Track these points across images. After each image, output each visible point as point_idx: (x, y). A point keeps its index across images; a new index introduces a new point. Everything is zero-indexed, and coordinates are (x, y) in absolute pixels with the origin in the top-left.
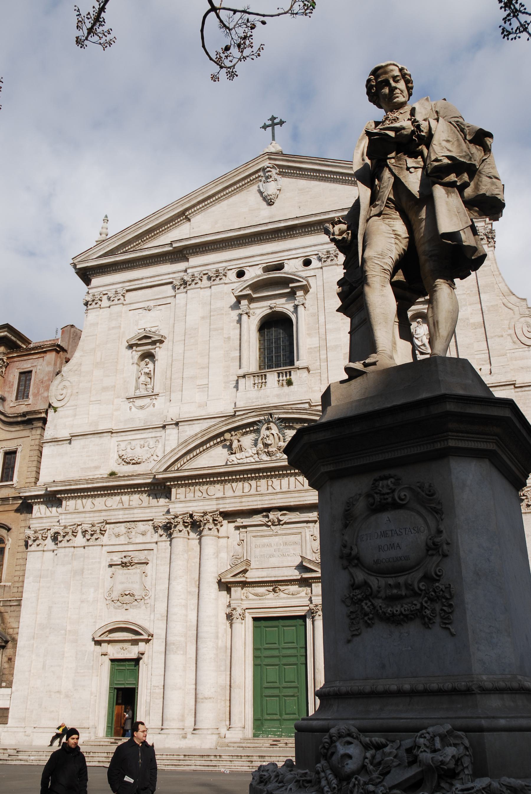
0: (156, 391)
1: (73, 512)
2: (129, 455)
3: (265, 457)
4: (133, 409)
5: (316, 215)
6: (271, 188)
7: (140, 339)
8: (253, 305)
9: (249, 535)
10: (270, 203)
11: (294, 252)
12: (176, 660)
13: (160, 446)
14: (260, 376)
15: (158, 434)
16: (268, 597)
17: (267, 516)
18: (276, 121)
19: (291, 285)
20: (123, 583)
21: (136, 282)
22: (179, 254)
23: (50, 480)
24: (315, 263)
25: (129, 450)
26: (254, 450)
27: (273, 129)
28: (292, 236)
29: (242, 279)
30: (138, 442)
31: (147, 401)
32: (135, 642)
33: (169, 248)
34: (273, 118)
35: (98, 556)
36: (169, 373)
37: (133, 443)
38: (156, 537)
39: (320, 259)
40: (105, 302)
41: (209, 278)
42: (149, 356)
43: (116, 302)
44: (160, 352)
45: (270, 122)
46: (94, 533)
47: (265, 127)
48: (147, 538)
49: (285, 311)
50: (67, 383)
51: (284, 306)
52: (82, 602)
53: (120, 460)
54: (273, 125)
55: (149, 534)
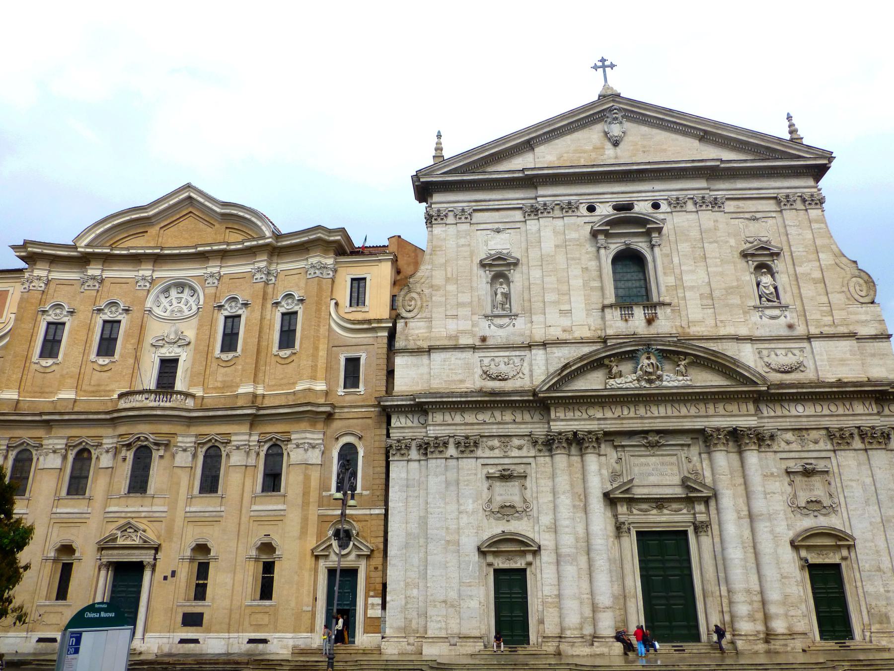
0: (514, 311)
1: (438, 426)
2: (493, 371)
3: (643, 384)
4: (492, 327)
5: (702, 161)
6: (615, 130)
7: (493, 260)
9: (627, 454)
10: (616, 144)
11: (644, 194)
12: (569, 571)
15: (523, 353)
16: (652, 512)
17: (647, 438)
18: (607, 63)
19: (648, 226)
20: (501, 495)
21: (483, 203)
23: (404, 388)
24: (664, 207)
25: (493, 366)
26: (634, 377)
27: (604, 71)
29: (593, 214)
30: (501, 359)
31: (506, 321)
32: (523, 553)
33: (521, 175)
34: (603, 60)
35: (471, 470)
37: (497, 360)
38: (533, 453)
39: (670, 204)
40: (451, 219)
41: (562, 209)
42: (762, 268)
43: (463, 220)
45: (600, 64)
46: (468, 446)
48: (524, 452)
49: (639, 248)
50: (414, 295)
51: (641, 245)
52: (460, 513)
53: (485, 376)
55: (525, 448)
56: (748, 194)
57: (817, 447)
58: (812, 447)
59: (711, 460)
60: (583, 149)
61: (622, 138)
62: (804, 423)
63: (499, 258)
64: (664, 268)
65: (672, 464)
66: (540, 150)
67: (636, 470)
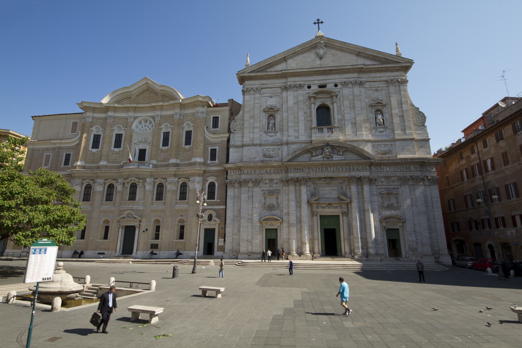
6: (321, 52)
8: (316, 100)
10: (321, 58)
13: (280, 151)
22: (284, 75)
24: (339, 86)
28: (331, 74)
34: (318, 20)
36: (281, 123)
39: (342, 84)
42: (379, 111)
44: (278, 117)
45: (317, 22)
47: (315, 23)
51: (328, 103)
54: (318, 23)
56: (375, 79)
57: (394, 184)
58: (391, 183)
60: (308, 61)
63: (379, 103)
65: (335, 190)
66: (290, 61)
67: (321, 192)
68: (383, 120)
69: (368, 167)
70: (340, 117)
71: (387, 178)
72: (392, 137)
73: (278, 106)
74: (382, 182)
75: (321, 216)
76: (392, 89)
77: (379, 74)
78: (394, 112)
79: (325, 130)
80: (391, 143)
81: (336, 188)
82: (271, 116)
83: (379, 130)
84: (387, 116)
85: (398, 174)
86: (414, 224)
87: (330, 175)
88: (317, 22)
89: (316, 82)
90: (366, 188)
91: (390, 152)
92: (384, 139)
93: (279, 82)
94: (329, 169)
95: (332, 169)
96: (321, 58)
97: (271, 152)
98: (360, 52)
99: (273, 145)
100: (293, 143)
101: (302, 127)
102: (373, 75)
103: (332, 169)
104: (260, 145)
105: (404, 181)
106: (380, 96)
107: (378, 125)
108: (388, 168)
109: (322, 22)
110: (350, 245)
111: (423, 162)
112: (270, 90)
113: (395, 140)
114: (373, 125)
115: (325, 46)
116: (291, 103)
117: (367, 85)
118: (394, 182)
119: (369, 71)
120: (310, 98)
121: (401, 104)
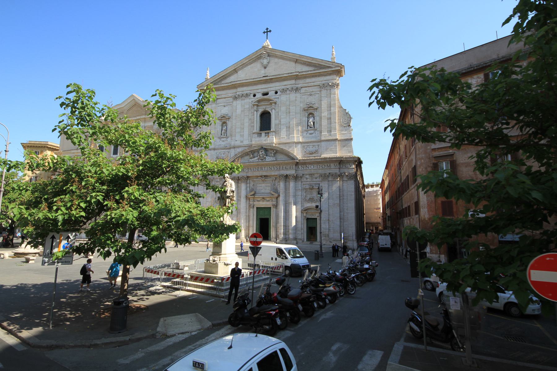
6: (265, 61)
14: (260, 135)
22: (234, 86)
34: (267, 29)
42: (311, 115)
44: (229, 123)
47: (264, 33)
54: (267, 32)
56: (310, 84)
58: (314, 180)
59: (368, 186)
60: (254, 71)
61: (267, 65)
62: (313, 172)
63: (224, 117)
64: (275, 117)
66: (240, 72)
67: (258, 188)
68: (314, 123)
69: (294, 166)
70: (277, 122)
71: (311, 175)
72: (319, 138)
73: (230, 115)
74: (307, 179)
75: (257, 208)
76: (324, 92)
77: (313, 79)
78: (323, 115)
79: (263, 134)
80: (318, 144)
81: (270, 185)
82: (224, 123)
83: (310, 132)
84: (317, 118)
85: (320, 171)
86: (329, 215)
87: (264, 174)
88: (266, 31)
89: (260, 91)
90: (292, 184)
91: (316, 152)
92: (312, 140)
93: (230, 93)
94: (264, 169)
95: (266, 168)
96: (265, 68)
97: (223, 155)
98: (298, 60)
99: (224, 149)
100: (238, 147)
101: (246, 132)
102: (308, 80)
103: (266, 168)
104: (214, 149)
105: (325, 177)
106: (312, 100)
107: (311, 128)
108: (312, 167)
109: (270, 31)
110: (277, 232)
111: (341, 161)
112: (224, 99)
113: (321, 141)
114: (305, 128)
115: (269, 56)
116: (239, 111)
117: (303, 90)
118: (316, 178)
119: (305, 77)
120: (254, 105)
121: (330, 106)
